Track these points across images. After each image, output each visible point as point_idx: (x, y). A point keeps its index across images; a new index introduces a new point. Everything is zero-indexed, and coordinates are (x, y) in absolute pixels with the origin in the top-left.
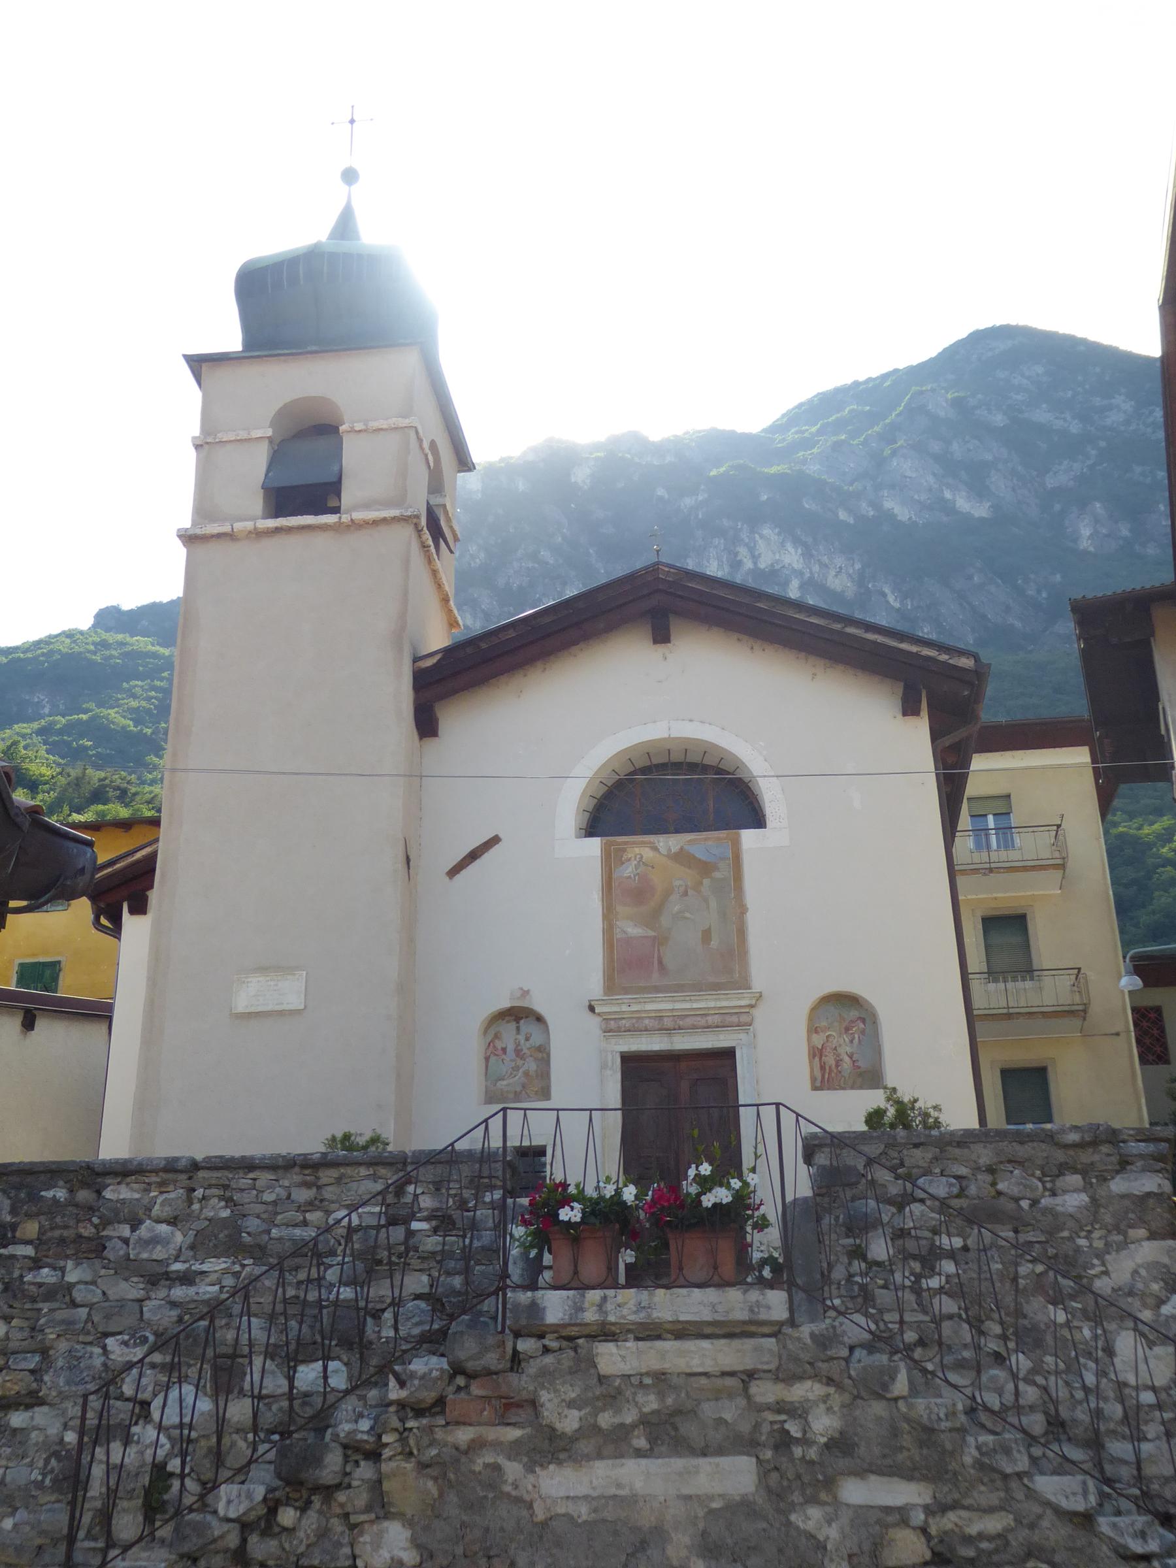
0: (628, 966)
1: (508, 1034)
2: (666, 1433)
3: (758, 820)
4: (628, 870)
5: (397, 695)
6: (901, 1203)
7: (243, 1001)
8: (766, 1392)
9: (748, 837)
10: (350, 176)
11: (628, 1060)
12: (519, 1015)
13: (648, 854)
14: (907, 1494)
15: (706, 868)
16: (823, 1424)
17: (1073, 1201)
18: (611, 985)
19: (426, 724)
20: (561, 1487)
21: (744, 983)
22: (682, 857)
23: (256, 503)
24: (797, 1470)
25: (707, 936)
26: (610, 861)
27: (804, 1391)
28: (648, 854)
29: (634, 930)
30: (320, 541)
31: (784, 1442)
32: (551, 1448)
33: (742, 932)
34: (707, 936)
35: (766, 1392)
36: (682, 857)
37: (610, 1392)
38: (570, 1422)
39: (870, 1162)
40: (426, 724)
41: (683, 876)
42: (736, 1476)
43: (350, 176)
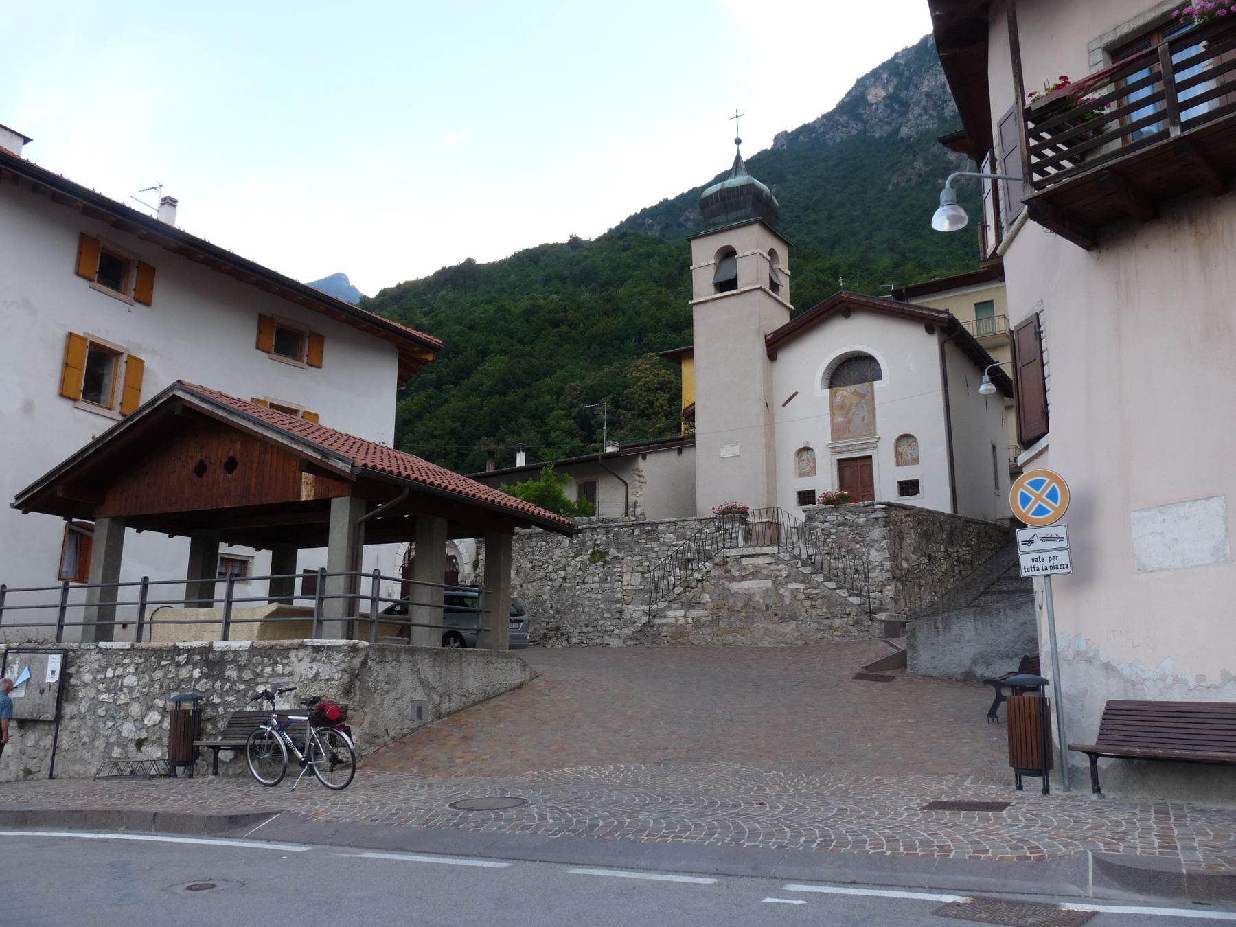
0: (838, 431)
1: (805, 456)
2: (755, 575)
3: (879, 377)
4: (838, 399)
5: (760, 349)
6: (823, 522)
7: (723, 453)
8: (773, 567)
9: (876, 384)
10: (738, 142)
11: (839, 461)
12: (807, 449)
13: (844, 393)
14: (801, 586)
15: (862, 396)
16: (784, 573)
17: (862, 520)
18: (833, 439)
19: (772, 356)
20: (735, 587)
21: (875, 433)
22: (855, 393)
23: (713, 289)
24: (778, 584)
25: (863, 419)
26: (833, 396)
27: (781, 566)
28: (844, 393)
29: (840, 419)
30: (732, 300)
31: (777, 577)
32: (733, 579)
33: (874, 416)
34: (863, 419)
35: (773, 567)
36: (855, 393)
37: (745, 568)
38: (737, 574)
39: (152, 681)
40: (772, 356)
41: (855, 400)
42: (768, 584)
43: (738, 142)
